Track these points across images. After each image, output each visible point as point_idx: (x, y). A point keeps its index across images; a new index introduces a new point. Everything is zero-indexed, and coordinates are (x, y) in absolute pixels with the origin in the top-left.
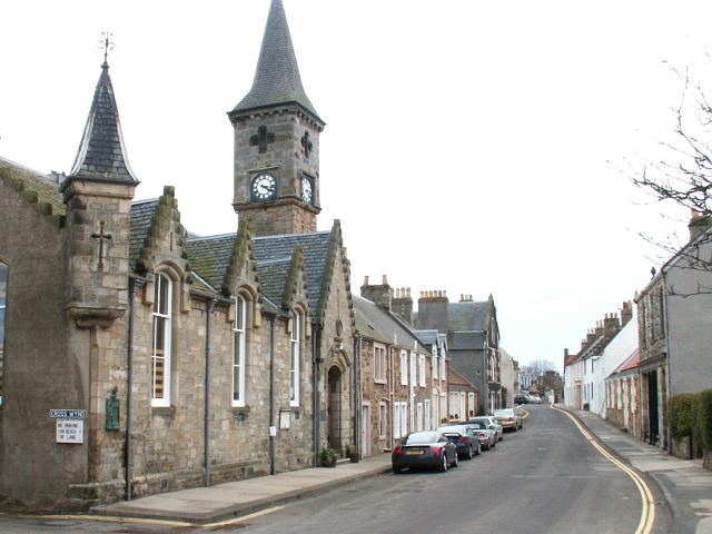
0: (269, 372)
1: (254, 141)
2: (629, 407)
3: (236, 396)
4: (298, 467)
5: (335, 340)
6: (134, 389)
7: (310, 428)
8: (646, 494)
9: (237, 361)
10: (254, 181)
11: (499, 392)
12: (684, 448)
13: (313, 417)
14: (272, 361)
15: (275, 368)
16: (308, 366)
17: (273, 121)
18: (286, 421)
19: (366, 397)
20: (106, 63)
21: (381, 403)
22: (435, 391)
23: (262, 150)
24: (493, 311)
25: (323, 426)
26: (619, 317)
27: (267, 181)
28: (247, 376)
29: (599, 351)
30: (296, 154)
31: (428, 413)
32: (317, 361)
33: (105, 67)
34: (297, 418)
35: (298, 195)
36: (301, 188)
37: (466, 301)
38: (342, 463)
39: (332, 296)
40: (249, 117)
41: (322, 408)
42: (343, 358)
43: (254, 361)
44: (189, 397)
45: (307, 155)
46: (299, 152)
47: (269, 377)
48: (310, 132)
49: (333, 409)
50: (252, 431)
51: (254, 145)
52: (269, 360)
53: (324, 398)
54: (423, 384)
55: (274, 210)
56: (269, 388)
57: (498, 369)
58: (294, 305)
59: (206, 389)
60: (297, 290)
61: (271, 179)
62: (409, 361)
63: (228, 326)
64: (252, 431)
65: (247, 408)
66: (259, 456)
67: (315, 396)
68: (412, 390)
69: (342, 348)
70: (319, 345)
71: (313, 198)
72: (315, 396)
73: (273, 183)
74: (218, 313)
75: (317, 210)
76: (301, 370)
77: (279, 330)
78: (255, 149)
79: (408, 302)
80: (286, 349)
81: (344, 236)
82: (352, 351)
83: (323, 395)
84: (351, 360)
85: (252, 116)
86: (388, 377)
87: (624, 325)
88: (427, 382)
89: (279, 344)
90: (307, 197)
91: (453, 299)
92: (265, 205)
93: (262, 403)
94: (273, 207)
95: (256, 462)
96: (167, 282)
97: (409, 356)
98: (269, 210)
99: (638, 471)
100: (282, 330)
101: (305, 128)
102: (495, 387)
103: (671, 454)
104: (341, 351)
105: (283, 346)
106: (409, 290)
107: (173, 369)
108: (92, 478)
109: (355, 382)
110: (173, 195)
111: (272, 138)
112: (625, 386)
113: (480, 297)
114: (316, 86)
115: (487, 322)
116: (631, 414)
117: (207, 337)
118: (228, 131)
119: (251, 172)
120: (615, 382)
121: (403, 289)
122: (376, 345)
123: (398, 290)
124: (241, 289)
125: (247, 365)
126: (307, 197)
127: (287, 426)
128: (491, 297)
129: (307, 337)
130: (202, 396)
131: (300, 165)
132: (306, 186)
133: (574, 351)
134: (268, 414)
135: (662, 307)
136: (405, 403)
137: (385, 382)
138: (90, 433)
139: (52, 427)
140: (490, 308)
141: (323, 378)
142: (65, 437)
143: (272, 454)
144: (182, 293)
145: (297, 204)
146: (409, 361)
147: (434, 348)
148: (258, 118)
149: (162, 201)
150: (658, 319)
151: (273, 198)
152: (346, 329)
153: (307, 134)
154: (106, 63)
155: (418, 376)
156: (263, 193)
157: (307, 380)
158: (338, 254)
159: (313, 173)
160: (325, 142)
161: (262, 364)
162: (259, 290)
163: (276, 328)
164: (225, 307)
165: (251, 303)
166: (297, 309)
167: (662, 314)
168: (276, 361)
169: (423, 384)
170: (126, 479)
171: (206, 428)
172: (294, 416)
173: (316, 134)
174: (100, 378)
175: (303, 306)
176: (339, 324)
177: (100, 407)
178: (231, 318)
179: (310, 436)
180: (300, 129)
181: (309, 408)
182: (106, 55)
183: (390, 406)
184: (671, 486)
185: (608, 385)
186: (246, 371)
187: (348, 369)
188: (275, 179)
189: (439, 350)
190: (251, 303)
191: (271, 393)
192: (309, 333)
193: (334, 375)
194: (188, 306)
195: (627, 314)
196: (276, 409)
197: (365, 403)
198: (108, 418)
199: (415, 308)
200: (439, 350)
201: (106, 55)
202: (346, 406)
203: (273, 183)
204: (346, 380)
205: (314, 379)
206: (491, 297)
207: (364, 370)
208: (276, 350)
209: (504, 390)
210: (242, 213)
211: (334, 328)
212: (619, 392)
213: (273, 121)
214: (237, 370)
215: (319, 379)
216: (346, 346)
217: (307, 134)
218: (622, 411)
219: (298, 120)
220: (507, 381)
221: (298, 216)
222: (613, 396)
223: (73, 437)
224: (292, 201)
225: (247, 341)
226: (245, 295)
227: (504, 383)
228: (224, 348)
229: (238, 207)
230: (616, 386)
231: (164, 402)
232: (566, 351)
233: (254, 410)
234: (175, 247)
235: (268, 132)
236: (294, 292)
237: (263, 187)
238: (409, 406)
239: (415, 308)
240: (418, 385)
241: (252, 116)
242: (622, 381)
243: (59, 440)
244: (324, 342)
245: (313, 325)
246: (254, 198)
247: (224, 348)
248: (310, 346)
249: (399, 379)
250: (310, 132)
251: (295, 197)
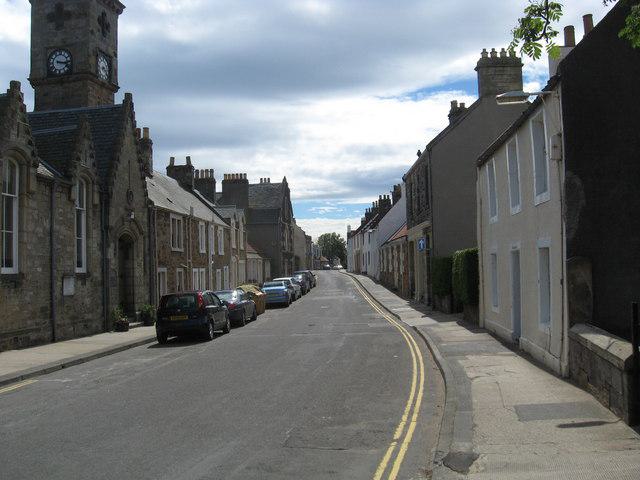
0: (48, 238)
1: (51, 18)
2: (399, 270)
3: (79, 265)
4: (85, 332)
5: (126, 209)
7: (100, 294)
8: (416, 352)
9: (79, 235)
10: (50, 57)
11: (292, 260)
12: (446, 303)
13: (103, 283)
14: (51, 227)
16: (96, 234)
18: (69, 288)
19: (162, 264)
21: (178, 270)
22: (233, 259)
23: (59, 27)
24: (287, 191)
25: (114, 293)
26: (391, 198)
27: (63, 57)
28: (20, 242)
29: (374, 225)
30: (92, 32)
31: (226, 277)
32: (106, 229)
34: (84, 284)
35: (93, 71)
36: (97, 65)
37: (265, 185)
38: (134, 327)
41: (112, 275)
42: (135, 227)
43: (30, 227)
45: (103, 33)
46: (95, 30)
47: (48, 244)
49: (125, 276)
50: (28, 299)
51: (51, 21)
52: (48, 227)
53: (114, 263)
54: (222, 253)
55: (71, 85)
57: (291, 241)
60: (82, 156)
61: (66, 55)
62: (207, 231)
64: (28, 299)
65: (21, 275)
66: (37, 324)
67: (105, 262)
68: (210, 258)
69: (132, 217)
70: (107, 213)
71: (110, 76)
72: (105, 262)
75: (116, 88)
76: (88, 237)
77: (60, 198)
78: (52, 26)
80: (69, 216)
81: (136, 109)
82: (145, 220)
83: (113, 261)
84: (145, 229)
86: (185, 246)
87: (394, 204)
91: (253, 180)
92: (61, 80)
93: (39, 270)
94: (69, 82)
95: (32, 330)
97: (207, 228)
99: (406, 326)
100: (64, 198)
101: (102, 8)
102: (289, 256)
103: (434, 308)
104: (133, 220)
106: (212, 171)
109: (149, 250)
112: (395, 252)
113: (276, 180)
115: (281, 200)
116: (400, 276)
119: (47, 49)
120: (387, 249)
125: (20, 231)
128: (285, 179)
129: (95, 206)
131: (96, 41)
132: (103, 64)
133: (355, 228)
134: (48, 281)
135: (427, 182)
136: (203, 270)
137: (182, 250)
140: (284, 188)
141: (112, 245)
143: (52, 323)
144: (93, 191)
145: (91, 80)
146: (207, 231)
147: (233, 221)
150: (424, 193)
151: (69, 73)
153: (104, 14)
155: (216, 246)
156: (60, 68)
157: (95, 246)
158: (129, 126)
159: (111, 52)
161: (40, 230)
162: (33, 154)
163: (56, 195)
165: (25, 167)
167: (427, 187)
168: (56, 227)
169: (222, 253)
172: (80, 283)
175: (89, 174)
176: (129, 194)
179: (100, 302)
181: (97, 274)
183: (188, 273)
184: (439, 341)
185: (381, 253)
186: (20, 237)
187: (141, 238)
188: (70, 55)
189: (237, 223)
190: (25, 167)
191: (51, 260)
192: (97, 201)
193: (126, 246)
194: (33, 186)
195: (397, 194)
196: (57, 275)
197: (160, 270)
199: (219, 188)
200: (237, 223)
202: (139, 272)
204: (140, 247)
205: (103, 247)
206: (285, 179)
208: (56, 216)
209: (297, 258)
211: (125, 197)
212: (390, 258)
214: (9, 237)
215: (109, 246)
217: (104, 14)
218: (392, 274)
220: (299, 251)
222: (385, 261)
225: (21, 206)
227: (296, 252)
230: (388, 253)
233: (29, 277)
236: (79, 159)
238: (207, 272)
239: (219, 188)
240: (217, 253)
242: (392, 249)
244: (113, 210)
245: (101, 194)
246: (50, 73)
248: (98, 214)
249: (197, 248)
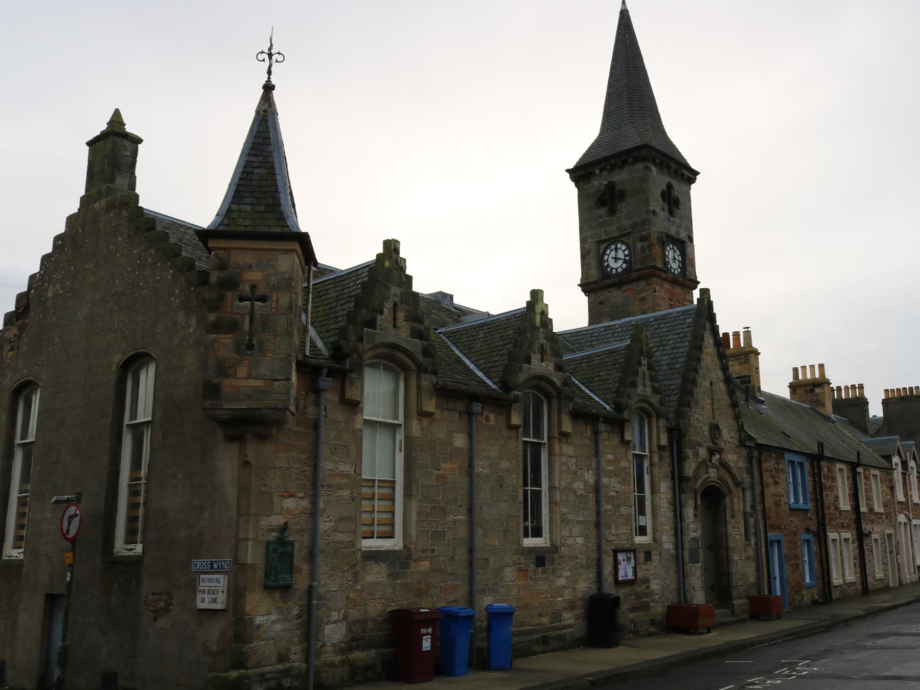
0: (592, 496)
6: (324, 525)
10: (604, 253)
15: (603, 491)
17: (632, 182)
20: (269, 80)
23: (612, 212)
30: (654, 212)
32: (679, 482)
33: (268, 88)
36: (664, 256)
39: (704, 384)
40: (593, 173)
44: (438, 536)
45: (671, 213)
47: (592, 504)
48: (674, 183)
56: (594, 518)
58: (633, 402)
59: (471, 524)
63: (513, 434)
65: (554, 548)
73: (627, 252)
74: (492, 416)
76: (653, 492)
78: (603, 211)
79: (861, 403)
85: (597, 171)
88: (885, 505)
89: (610, 457)
90: (675, 266)
96: (644, 419)
98: (625, 287)
100: (615, 441)
105: (616, 461)
106: (861, 387)
107: (407, 495)
108: (239, 662)
110: (397, 251)
111: (622, 196)
114: (684, 126)
117: (471, 449)
118: (571, 191)
121: (853, 387)
122: (788, 457)
123: (846, 387)
124: (641, 404)
125: (551, 488)
126: (675, 266)
127: (630, 576)
129: (661, 448)
130: (462, 533)
131: (661, 223)
132: (672, 254)
138: (236, 594)
139: (192, 587)
142: (206, 601)
145: (659, 277)
147: (896, 460)
148: (605, 173)
149: (531, 305)
151: (626, 271)
152: (728, 435)
154: (269, 80)
159: (683, 235)
160: (699, 195)
164: (618, 424)
166: (642, 409)
168: (605, 480)
170: (307, 660)
171: (471, 577)
173: (683, 187)
174: (253, 511)
176: (715, 429)
177: (253, 555)
178: (628, 437)
180: (658, 180)
181: (668, 544)
182: (269, 72)
186: (551, 496)
188: (628, 247)
192: (664, 441)
193: (713, 499)
196: (607, 548)
198: (270, 570)
200: (904, 464)
201: (269, 72)
203: (627, 252)
207: (770, 491)
210: (593, 295)
213: (632, 182)
216: (734, 458)
217: (670, 187)
219: (654, 169)
221: (661, 291)
223: (214, 601)
224: (661, 273)
225: (550, 454)
226: (646, 414)
228: (505, 464)
229: (586, 287)
231: (395, 544)
232: (113, 152)
234: (648, 382)
235: (617, 188)
237: (616, 259)
241: (597, 171)
243: (201, 606)
245: (670, 431)
247: (505, 464)
250: (674, 183)
251: (655, 268)
